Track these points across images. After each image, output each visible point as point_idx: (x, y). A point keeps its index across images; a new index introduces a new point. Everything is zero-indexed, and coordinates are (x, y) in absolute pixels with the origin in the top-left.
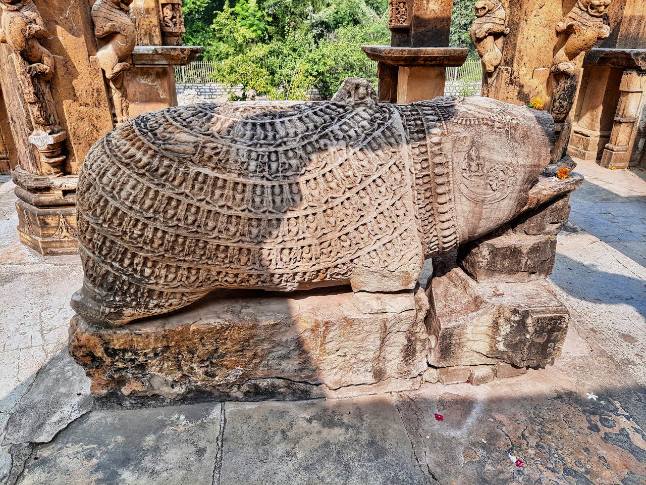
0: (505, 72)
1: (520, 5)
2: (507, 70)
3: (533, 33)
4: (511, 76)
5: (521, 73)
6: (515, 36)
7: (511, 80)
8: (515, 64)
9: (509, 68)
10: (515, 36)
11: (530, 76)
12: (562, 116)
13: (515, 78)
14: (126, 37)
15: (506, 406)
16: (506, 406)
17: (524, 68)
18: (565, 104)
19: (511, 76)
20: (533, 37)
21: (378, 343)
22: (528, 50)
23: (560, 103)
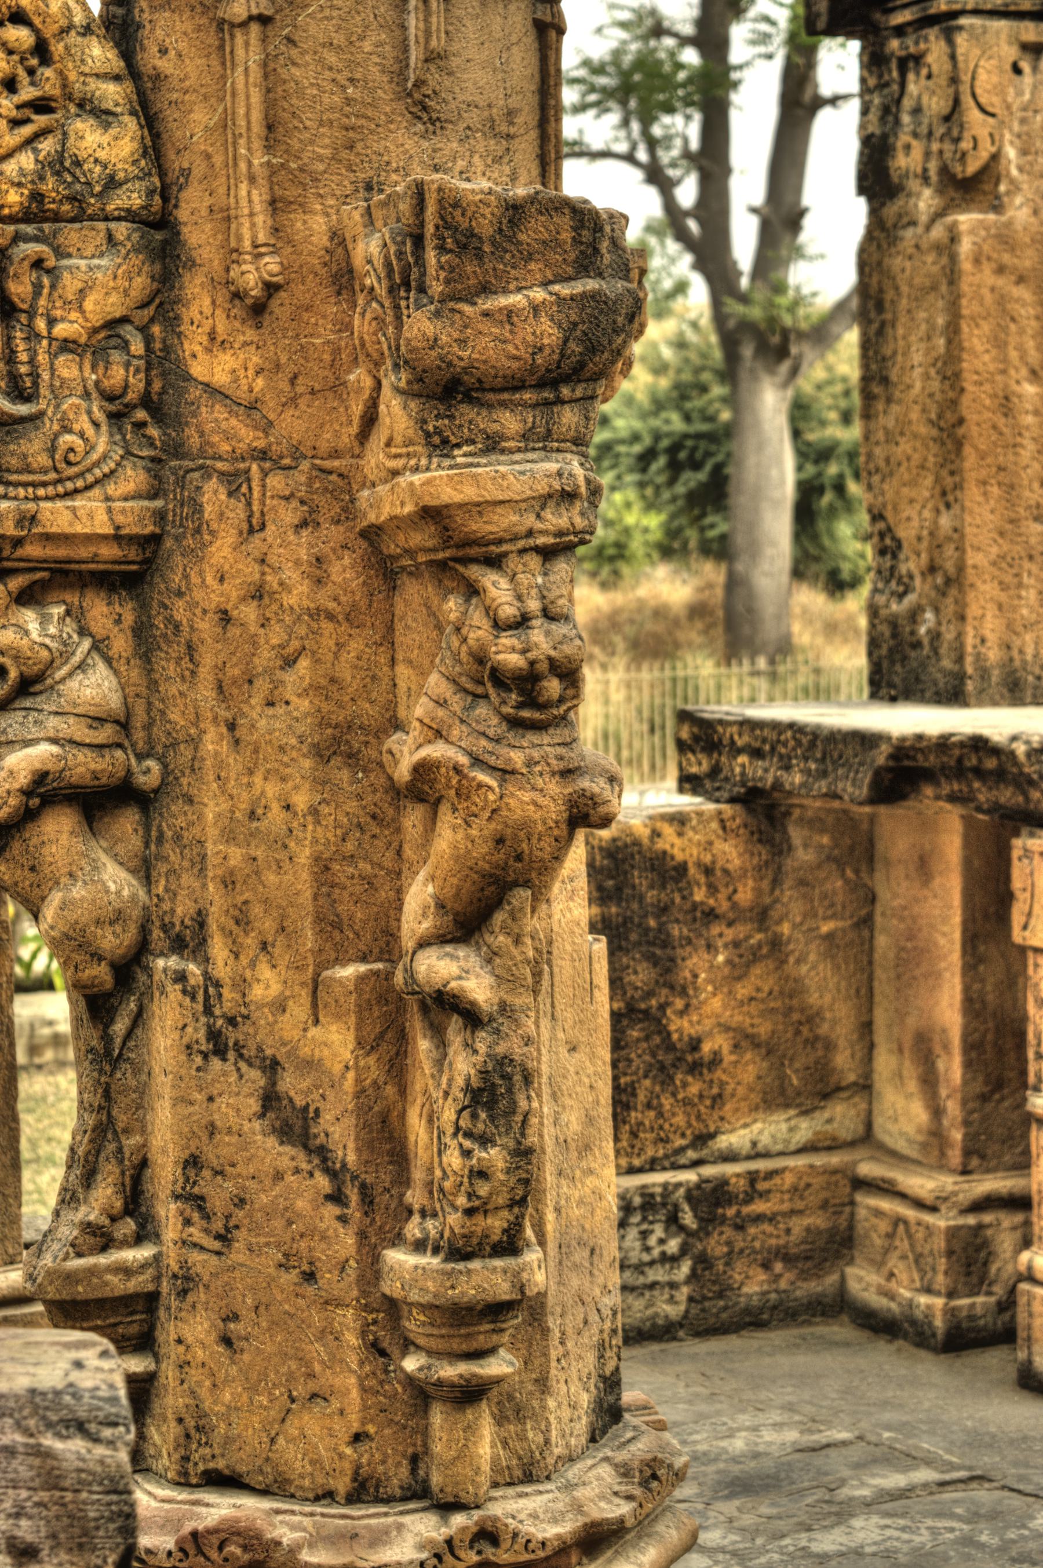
0: (174, 992)
1: (190, 648)
2: (181, 977)
3: (272, 789)
4: (208, 1010)
5: (257, 992)
6: (190, 800)
7: (214, 1035)
8: (218, 949)
9: (193, 968)
10: (190, 800)
11: (299, 1010)
12: (496, 1224)
13: (232, 1021)
14: (787, 979)
15: (398, 1492)
16: (398, 1492)
17: (265, 972)
18: (495, 1157)
19: (208, 1010)
20: (275, 807)
21: (499, 510)
22: (271, 878)
23: (467, 1154)
